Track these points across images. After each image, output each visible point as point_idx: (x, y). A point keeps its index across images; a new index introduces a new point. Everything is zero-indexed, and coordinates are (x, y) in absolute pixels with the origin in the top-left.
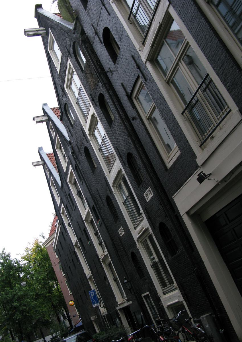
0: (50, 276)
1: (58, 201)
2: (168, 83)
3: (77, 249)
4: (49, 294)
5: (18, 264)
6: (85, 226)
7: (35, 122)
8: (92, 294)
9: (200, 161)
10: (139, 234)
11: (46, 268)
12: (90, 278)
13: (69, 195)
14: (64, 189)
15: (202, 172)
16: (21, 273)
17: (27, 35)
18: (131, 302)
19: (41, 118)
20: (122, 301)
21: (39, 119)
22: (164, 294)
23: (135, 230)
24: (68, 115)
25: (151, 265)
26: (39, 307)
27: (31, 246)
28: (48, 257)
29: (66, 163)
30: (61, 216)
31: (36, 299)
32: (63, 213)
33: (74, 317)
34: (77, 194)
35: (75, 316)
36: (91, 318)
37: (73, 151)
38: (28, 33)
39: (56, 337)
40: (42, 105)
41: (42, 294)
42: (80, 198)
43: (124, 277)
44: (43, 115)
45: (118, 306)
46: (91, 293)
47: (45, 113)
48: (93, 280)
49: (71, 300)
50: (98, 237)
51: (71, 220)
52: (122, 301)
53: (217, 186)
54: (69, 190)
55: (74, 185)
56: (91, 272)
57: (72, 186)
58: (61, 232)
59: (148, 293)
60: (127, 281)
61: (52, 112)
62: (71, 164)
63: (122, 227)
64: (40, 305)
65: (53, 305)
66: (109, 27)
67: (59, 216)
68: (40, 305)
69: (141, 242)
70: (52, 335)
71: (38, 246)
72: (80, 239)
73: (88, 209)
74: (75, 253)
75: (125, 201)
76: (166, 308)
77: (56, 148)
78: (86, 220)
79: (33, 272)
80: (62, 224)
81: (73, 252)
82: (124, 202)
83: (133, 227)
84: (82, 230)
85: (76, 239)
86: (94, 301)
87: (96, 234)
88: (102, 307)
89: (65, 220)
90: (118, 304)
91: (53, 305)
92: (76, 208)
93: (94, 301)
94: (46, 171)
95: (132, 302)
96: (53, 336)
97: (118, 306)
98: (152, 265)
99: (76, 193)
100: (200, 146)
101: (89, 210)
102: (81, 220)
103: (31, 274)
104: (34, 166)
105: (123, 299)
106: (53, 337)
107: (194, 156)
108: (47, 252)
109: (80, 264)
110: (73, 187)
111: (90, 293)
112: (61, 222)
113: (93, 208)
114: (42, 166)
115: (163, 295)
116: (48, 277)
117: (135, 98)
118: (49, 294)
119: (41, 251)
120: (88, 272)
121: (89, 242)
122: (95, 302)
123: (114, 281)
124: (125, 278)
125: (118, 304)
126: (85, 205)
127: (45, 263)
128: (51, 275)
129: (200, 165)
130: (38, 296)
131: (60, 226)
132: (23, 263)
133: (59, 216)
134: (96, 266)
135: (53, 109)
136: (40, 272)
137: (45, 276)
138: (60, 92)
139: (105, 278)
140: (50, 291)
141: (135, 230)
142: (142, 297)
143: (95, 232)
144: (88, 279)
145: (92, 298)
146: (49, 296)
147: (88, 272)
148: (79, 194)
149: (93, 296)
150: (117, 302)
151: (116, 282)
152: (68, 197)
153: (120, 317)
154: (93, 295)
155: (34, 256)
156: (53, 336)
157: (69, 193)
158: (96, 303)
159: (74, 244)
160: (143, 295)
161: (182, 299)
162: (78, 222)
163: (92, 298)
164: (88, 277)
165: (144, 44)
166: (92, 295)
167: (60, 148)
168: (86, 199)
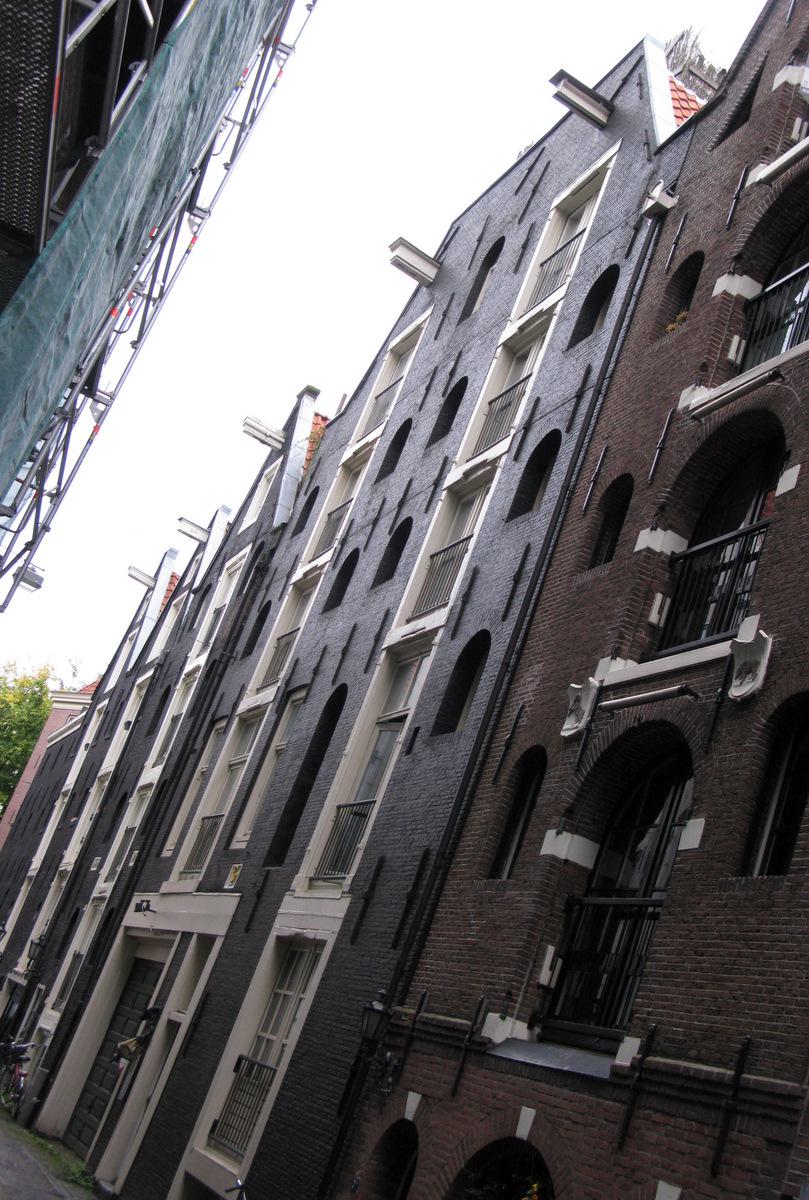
2: (230, 766)
3: (98, 790)
7: (554, 89)
9: (165, 887)
11: (11, 751)
12: (30, 878)
13: (122, 704)
15: (148, 902)
17: (396, 253)
19: (194, 529)
21: (187, 528)
27: (28, 670)
28: (39, 732)
30: (94, 711)
32: (140, 687)
38: (402, 253)
51: (137, 721)
53: (148, 930)
57: (136, 697)
66: (414, 519)
77: (174, 602)
85: (112, 769)
90: (16, 969)
94: (263, 480)
100: (311, 879)
107: (167, 878)
108: (46, 719)
109: (42, 834)
110: (135, 700)
117: (293, 702)
119: (38, 702)
120: (37, 862)
125: (16, 969)
127: (19, 738)
129: (162, 890)
131: (79, 726)
138: (218, 565)
147: (37, 862)
150: (16, 965)
159: (100, 774)
161: (53, 1031)
165: (408, 621)
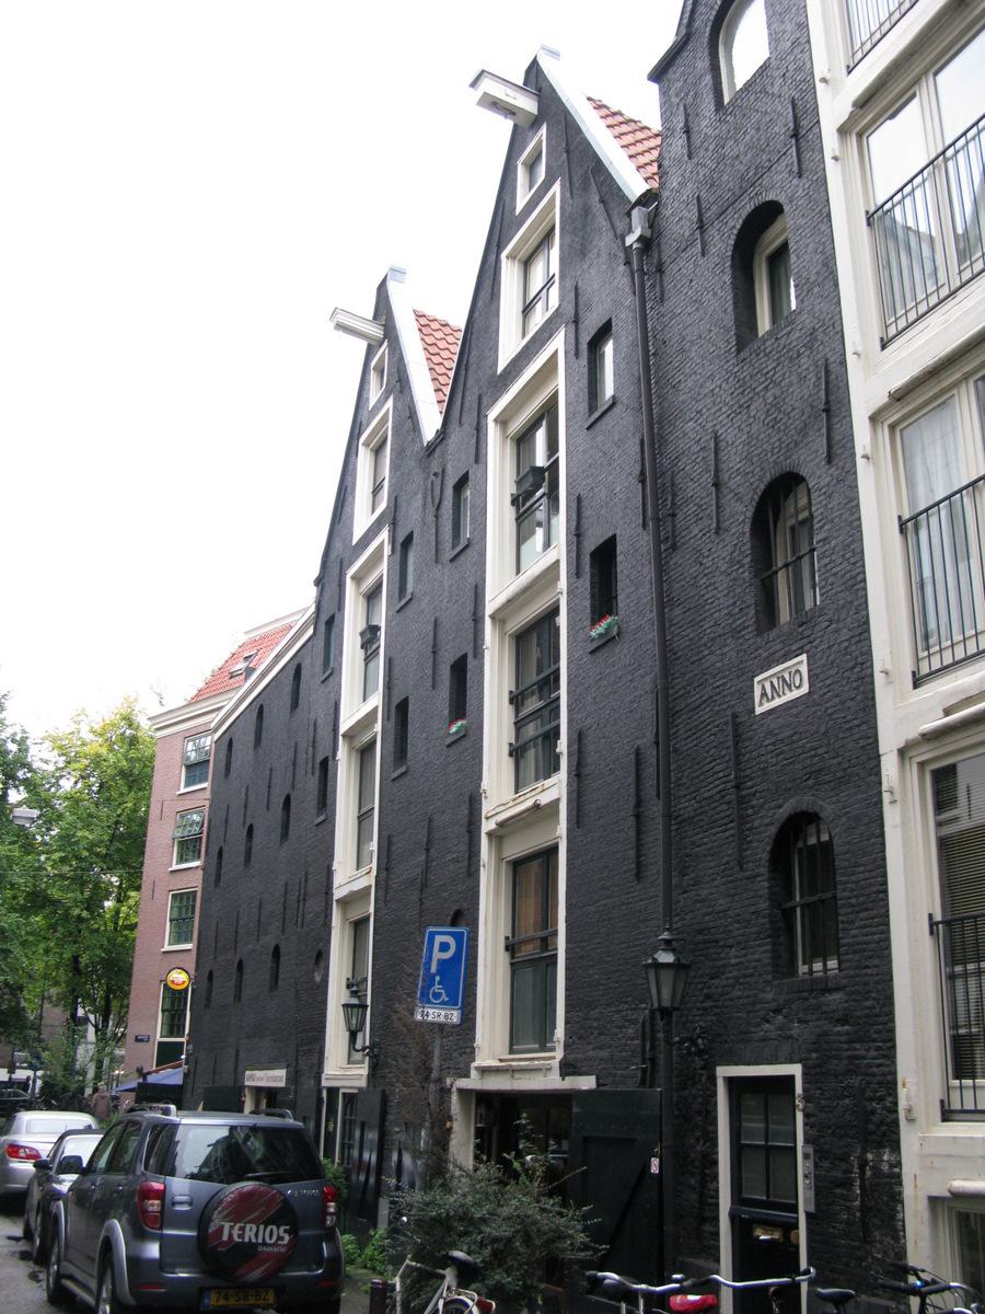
0: (120, 849)
1: (362, 518)
4: (85, 914)
5: (23, 749)
6: (334, 755)
8: (444, 947)
10: (947, 712)
11: (119, 811)
14: (443, 456)
16: (16, 787)
18: (587, 1083)
20: (501, 1060)
22: (947, 1115)
23: (916, 686)
24: (718, 38)
25: (930, 916)
26: (24, 944)
29: (524, 335)
31: (24, 911)
33: (137, 1040)
34: (362, 634)
35: (142, 1040)
36: (247, 1072)
37: (649, 232)
39: (24, 1085)
40: (540, 46)
41: (55, 903)
42: (518, 509)
43: (665, 935)
44: (521, 84)
45: (467, 1075)
46: (439, 939)
47: (533, 79)
48: (372, 910)
49: (180, 966)
50: (364, 810)
52: (501, 1060)
54: (479, 456)
55: (365, 604)
56: (374, 872)
58: (227, 737)
59: (795, 1070)
60: (678, 959)
61: (415, 326)
62: (394, 525)
63: (804, 657)
64: (31, 938)
65: (76, 959)
67: (331, 588)
68: (31, 938)
69: (922, 765)
70: (11, 1071)
71: (129, 721)
72: (403, 707)
73: (376, 700)
74: (326, 768)
75: (915, 517)
76: (923, 1205)
78: (349, 736)
79: (60, 805)
80: (322, 628)
81: (318, 760)
82: (906, 516)
83: (907, 667)
84: (448, 658)
86: (437, 988)
87: (517, 697)
88: (359, 1045)
89: (356, 612)
91: (76, 959)
92: (331, 679)
93: (437, 988)
95: (598, 1084)
96: (13, 1076)
97: (467, 1075)
98: (938, 917)
99: (360, 629)
101: (558, 562)
102: (470, 607)
103: (52, 807)
104: (340, 327)
105: (511, 1051)
106: (10, 1078)
111: (432, 936)
112: (324, 617)
113: (594, 555)
114: (363, 345)
115: (939, 1119)
116: (113, 848)
118: (85, 914)
119: (133, 741)
121: (459, 723)
122: (437, 996)
123: (507, 948)
124: (667, 942)
126: (524, 548)
128: (128, 848)
130: (38, 900)
131: (310, 632)
132: (43, 758)
133: (331, 588)
134: (428, 850)
135: (425, 323)
136: (90, 815)
137: (102, 842)
139: (321, 957)
140: (93, 904)
141: (916, 686)
142: (713, 1079)
143: (517, 687)
144: (337, 901)
145: (434, 969)
146: (80, 919)
148: (370, 635)
149: (442, 963)
151: (513, 957)
152: (449, 492)
153: (450, 1130)
154: (447, 955)
155: (96, 746)
156: (13, 1076)
157: (467, 472)
158: (443, 1003)
160: (723, 1072)
162: (436, 623)
163: (434, 969)
164: (338, 894)
166: (437, 955)
167: (378, 451)
168: (390, 663)
